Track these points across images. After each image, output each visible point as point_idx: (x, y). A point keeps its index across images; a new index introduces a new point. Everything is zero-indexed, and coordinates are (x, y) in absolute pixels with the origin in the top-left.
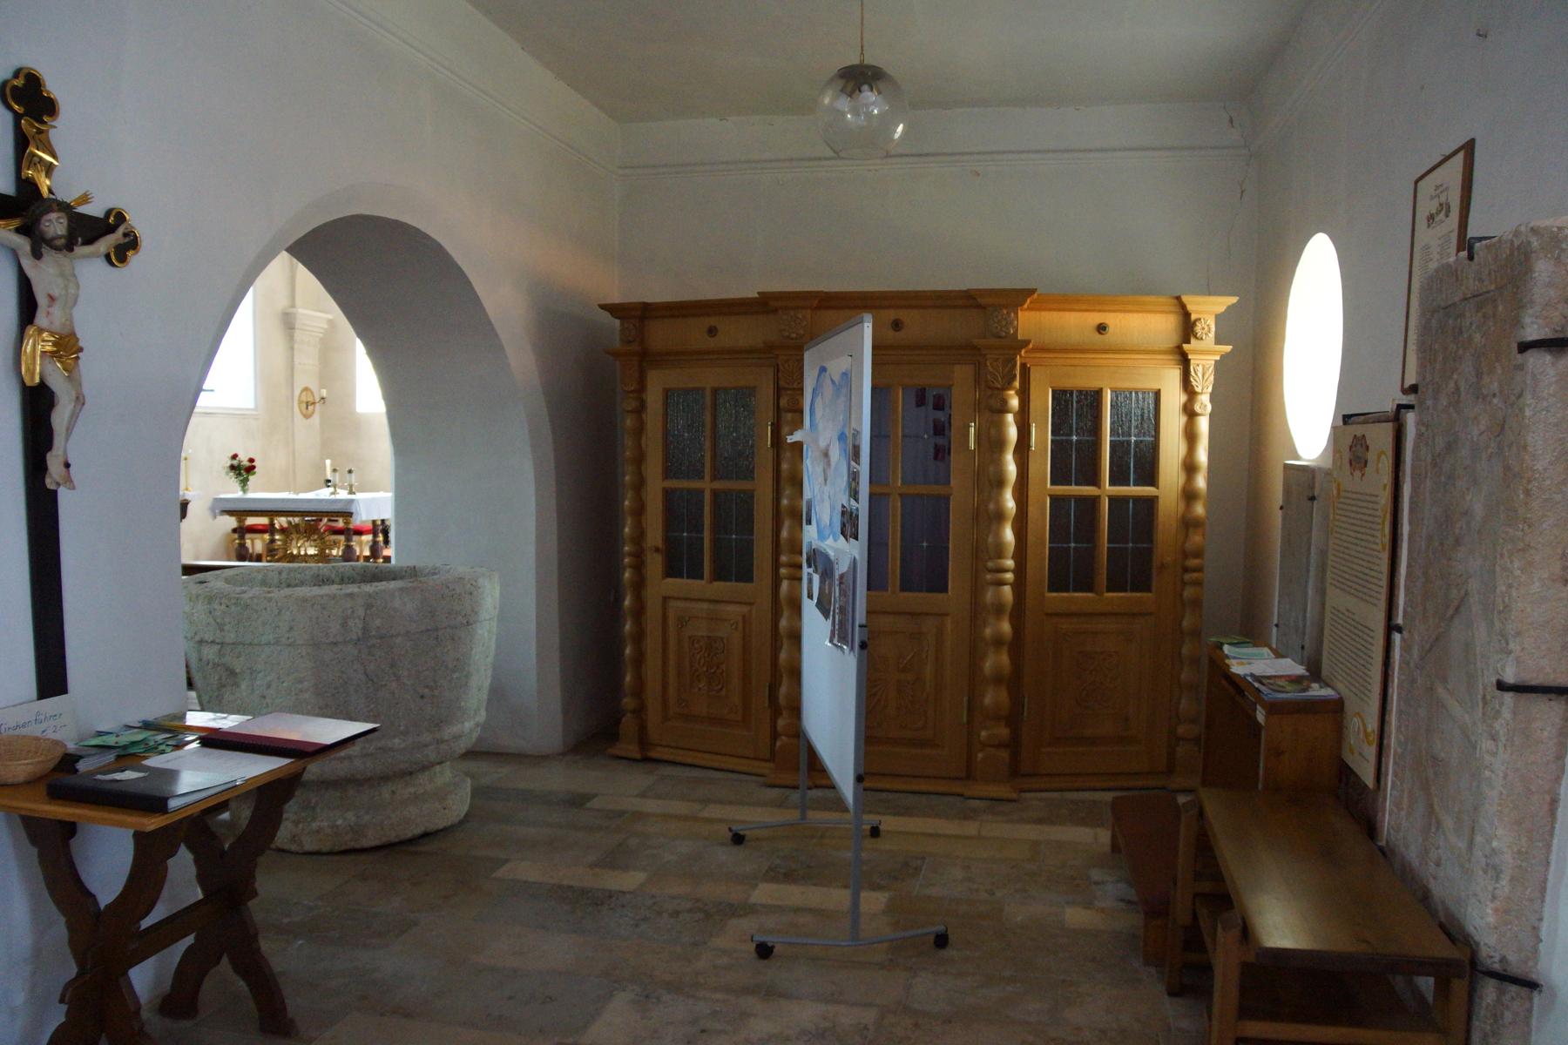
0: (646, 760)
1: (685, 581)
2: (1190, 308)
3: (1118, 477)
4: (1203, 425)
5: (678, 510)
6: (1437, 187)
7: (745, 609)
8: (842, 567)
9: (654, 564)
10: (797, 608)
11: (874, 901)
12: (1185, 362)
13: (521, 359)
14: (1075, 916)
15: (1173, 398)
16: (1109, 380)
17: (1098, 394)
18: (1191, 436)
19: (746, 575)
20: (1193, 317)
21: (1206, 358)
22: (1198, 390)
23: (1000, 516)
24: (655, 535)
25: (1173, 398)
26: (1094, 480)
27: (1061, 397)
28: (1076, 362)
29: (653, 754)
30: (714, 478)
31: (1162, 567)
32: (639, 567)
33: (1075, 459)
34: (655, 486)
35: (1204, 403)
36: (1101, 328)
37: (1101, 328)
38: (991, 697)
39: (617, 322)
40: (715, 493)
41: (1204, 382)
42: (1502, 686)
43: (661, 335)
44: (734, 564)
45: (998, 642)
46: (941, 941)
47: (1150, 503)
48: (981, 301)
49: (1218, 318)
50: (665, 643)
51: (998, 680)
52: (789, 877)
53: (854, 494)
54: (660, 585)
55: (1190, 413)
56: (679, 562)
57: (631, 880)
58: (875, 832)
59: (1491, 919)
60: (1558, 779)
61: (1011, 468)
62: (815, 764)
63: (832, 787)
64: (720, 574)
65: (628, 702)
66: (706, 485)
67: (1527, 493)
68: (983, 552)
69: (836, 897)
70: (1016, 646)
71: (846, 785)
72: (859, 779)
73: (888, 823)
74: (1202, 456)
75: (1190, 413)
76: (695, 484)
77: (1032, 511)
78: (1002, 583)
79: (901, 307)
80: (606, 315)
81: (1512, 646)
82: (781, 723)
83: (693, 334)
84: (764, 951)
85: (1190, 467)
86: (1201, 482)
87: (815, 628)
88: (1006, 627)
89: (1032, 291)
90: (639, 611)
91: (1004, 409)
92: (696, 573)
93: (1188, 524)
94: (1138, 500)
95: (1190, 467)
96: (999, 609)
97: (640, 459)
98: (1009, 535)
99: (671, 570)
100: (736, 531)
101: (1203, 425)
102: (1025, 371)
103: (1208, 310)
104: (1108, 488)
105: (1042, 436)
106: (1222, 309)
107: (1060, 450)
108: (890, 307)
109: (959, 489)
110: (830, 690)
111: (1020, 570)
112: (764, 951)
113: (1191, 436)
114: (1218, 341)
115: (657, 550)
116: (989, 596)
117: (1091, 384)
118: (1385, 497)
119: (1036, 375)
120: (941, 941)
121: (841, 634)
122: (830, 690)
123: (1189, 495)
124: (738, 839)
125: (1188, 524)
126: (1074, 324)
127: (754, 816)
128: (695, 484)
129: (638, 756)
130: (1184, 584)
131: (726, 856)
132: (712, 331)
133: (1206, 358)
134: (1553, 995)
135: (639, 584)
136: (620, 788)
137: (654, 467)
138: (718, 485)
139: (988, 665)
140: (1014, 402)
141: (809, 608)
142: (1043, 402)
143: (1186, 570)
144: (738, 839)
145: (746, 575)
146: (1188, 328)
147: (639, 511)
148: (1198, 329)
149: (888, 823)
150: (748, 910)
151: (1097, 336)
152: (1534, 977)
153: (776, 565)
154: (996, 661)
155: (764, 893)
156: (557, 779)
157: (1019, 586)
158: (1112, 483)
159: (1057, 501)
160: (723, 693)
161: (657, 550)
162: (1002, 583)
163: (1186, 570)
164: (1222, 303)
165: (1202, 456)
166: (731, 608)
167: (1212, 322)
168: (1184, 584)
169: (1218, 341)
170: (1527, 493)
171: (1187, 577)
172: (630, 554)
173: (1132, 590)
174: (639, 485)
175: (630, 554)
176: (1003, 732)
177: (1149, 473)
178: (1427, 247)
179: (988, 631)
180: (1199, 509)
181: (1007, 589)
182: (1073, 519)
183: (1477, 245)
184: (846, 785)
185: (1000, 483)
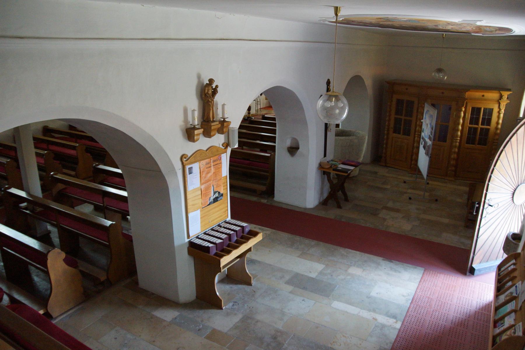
0: (386, 166)
3: (483, 124)
4: (502, 115)
5: (397, 121)
8: (428, 144)
9: (391, 130)
10: (418, 148)
11: (427, 194)
12: (499, 104)
13: (370, 91)
14: (459, 200)
15: (496, 110)
16: (483, 106)
17: (480, 109)
23: (458, 130)
24: (392, 125)
26: (478, 124)
27: (473, 109)
32: (388, 131)
33: (474, 120)
34: (393, 117)
35: (503, 111)
36: (483, 96)
37: (483, 96)
38: (453, 162)
40: (405, 120)
44: (407, 133)
45: (455, 152)
46: (436, 200)
47: (488, 130)
51: (454, 159)
52: (413, 189)
53: (431, 134)
54: (392, 135)
56: (396, 130)
57: (385, 187)
58: (428, 184)
61: (461, 121)
62: (419, 172)
63: (422, 175)
64: (404, 134)
66: (403, 117)
68: (454, 136)
69: (421, 193)
70: (458, 153)
71: (425, 176)
72: (427, 176)
73: (430, 182)
75: (499, 113)
76: (401, 117)
77: (465, 129)
78: (457, 142)
82: (413, 162)
84: (410, 198)
85: (498, 123)
86: (499, 126)
87: (422, 152)
88: (457, 150)
90: (387, 139)
91: (461, 111)
92: (399, 133)
93: (496, 134)
95: (498, 123)
96: (456, 147)
98: (459, 133)
99: (394, 132)
100: (409, 128)
101: (502, 115)
102: (467, 103)
104: (480, 126)
105: (468, 116)
107: (471, 119)
109: (451, 125)
110: (423, 161)
111: (461, 140)
112: (410, 198)
113: (499, 117)
116: (454, 144)
117: (480, 107)
119: (469, 104)
120: (436, 200)
121: (427, 154)
122: (423, 161)
123: (497, 128)
125: (496, 134)
126: (478, 94)
127: (407, 178)
128: (401, 117)
132: (407, 89)
133: (504, 103)
135: (388, 134)
136: (382, 171)
137: (393, 112)
138: (405, 118)
139: (452, 156)
140: (463, 109)
141: (421, 147)
142: (470, 109)
144: (405, 182)
145: (409, 135)
146: (501, 97)
147: (389, 120)
149: (430, 182)
150: (406, 193)
153: (415, 134)
154: (454, 156)
155: (409, 191)
156: (369, 168)
157: (460, 142)
159: (470, 128)
162: (457, 142)
165: (501, 121)
174: (390, 116)
176: (454, 168)
177: (489, 123)
179: (453, 150)
180: (498, 131)
181: (458, 143)
182: (472, 132)
184: (425, 176)
185: (459, 124)
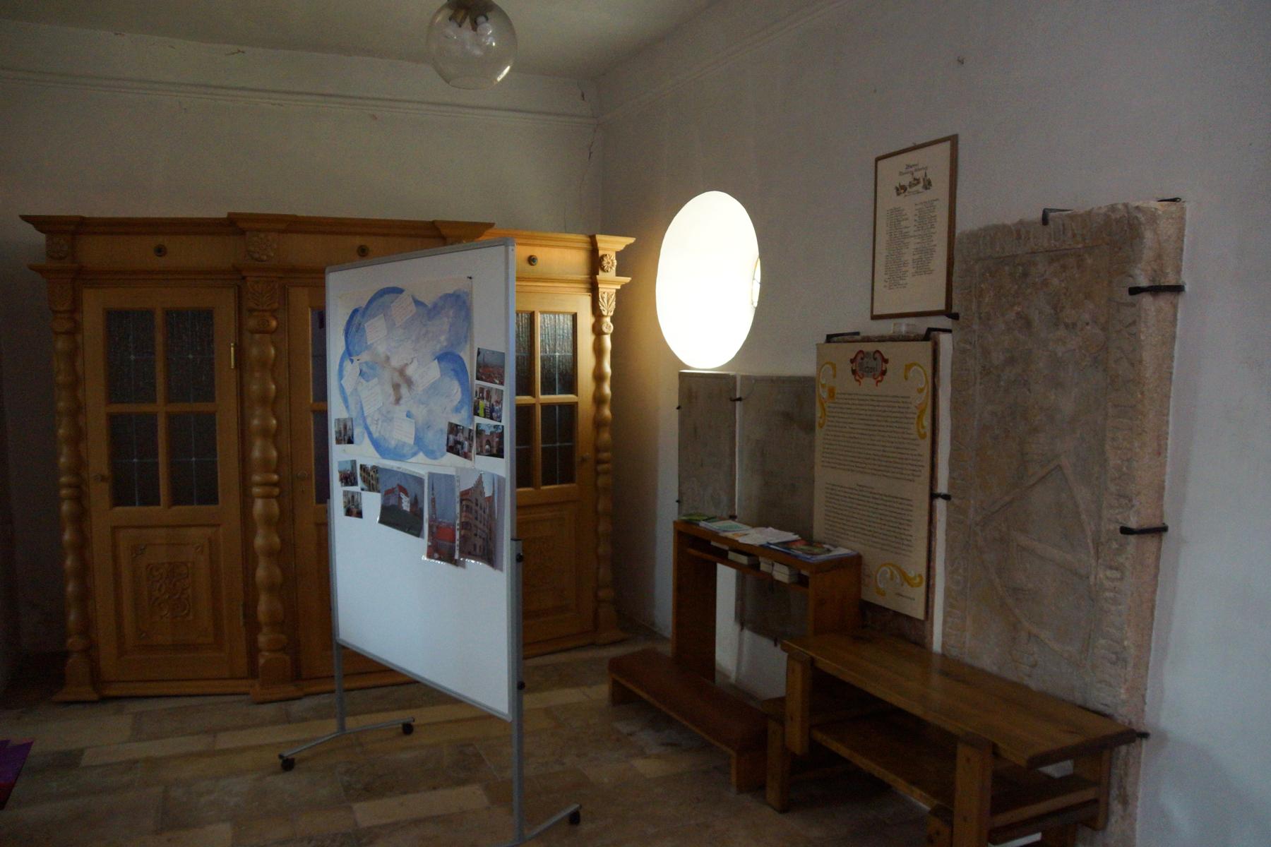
0: (105, 699)
1: (196, 507)
2: (600, 245)
5: (127, 437)
6: (909, 166)
7: (209, 531)
9: (100, 495)
12: (593, 289)
18: (598, 350)
19: (210, 497)
20: (601, 253)
21: (610, 284)
22: (605, 313)
24: (98, 459)
25: (586, 321)
28: (528, 289)
29: (113, 692)
30: (169, 400)
31: (584, 460)
32: (80, 497)
39: (42, 238)
40: (171, 418)
41: (608, 308)
42: (1126, 531)
43: (95, 252)
47: (571, 408)
48: (444, 232)
49: (618, 254)
50: (117, 575)
55: (598, 331)
56: (126, 490)
59: (1123, 697)
60: (1154, 592)
65: (74, 642)
67: (1142, 393)
74: (607, 368)
79: (369, 234)
80: (30, 228)
81: (1134, 502)
83: (139, 252)
86: (607, 389)
89: (491, 225)
90: (82, 544)
94: (562, 406)
95: (598, 377)
97: (76, 383)
99: (121, 497)
103: (611, 246)
106: (621, 247)
108: (356, 234)
114: (619, 273)
115: (103, 479)
118: (926, 397)
123: (599, 400)
124: (288, 765)
128: (146, 408)
129: (95, 697)
130: (598, 473)
131: (284, 783)
134: (1163, 738)
135: (81, 516)
137: (94, 392)
143: (599, 462)
144: (288, 765)
145: (210, 497)
146: (595, 263)
147: (78, 437)
148: (605, 263)
151: (528, 267)
152: (1143, 729)
158: (544, 393)
160: (191, 617)
161: (103, 479)
163: (599, 462)
164: (620, 243)
166: (193, 531)
167: (613, 257)
168: (598, 473)
169: (619, 273)
170: (1142, 393)
171: (601, 467)
172: (69, 486)
173: (561, 482)
174: (77, 410)
175: (69, 486)
177: (570, 383)
178: (897, 215)
183: (1052, 214)
